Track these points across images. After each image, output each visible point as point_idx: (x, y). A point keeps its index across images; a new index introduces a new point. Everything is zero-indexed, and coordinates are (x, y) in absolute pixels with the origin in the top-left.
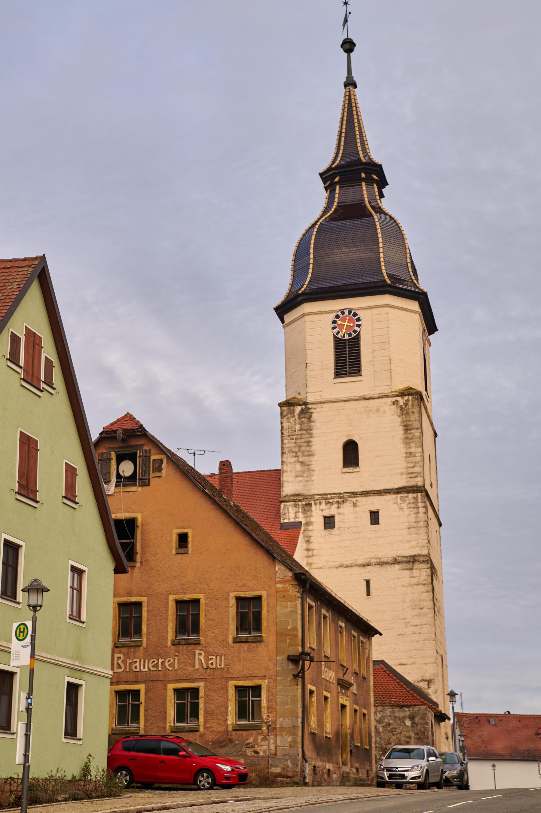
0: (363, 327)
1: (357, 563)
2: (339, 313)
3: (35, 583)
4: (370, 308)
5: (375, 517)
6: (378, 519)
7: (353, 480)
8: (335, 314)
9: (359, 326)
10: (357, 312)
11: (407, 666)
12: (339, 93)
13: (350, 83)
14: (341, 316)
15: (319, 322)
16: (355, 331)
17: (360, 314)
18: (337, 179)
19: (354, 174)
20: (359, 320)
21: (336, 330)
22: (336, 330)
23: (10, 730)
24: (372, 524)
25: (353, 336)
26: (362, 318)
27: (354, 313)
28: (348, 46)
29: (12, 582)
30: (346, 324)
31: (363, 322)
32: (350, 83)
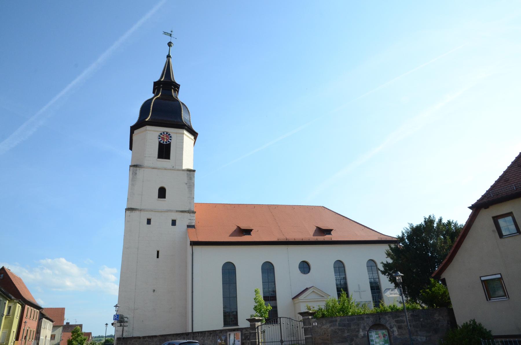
1: (139, 212)
3: (78, 327)
4: (176, 133)
5: (149, 222)
7: (162, 204)
9: (171, 139)
11: (142, 213)
13: (169, 56)
15: (152, 135)
17: (172, 135)
19: (166, 86)
20: (171, 137)
21: (160, 139)
22: (160, 139)
23: (237, 324)
24: (172, 225)
28: (170, 44)
29: (19, 315)
31: (173, 138)
32: (169, 56)
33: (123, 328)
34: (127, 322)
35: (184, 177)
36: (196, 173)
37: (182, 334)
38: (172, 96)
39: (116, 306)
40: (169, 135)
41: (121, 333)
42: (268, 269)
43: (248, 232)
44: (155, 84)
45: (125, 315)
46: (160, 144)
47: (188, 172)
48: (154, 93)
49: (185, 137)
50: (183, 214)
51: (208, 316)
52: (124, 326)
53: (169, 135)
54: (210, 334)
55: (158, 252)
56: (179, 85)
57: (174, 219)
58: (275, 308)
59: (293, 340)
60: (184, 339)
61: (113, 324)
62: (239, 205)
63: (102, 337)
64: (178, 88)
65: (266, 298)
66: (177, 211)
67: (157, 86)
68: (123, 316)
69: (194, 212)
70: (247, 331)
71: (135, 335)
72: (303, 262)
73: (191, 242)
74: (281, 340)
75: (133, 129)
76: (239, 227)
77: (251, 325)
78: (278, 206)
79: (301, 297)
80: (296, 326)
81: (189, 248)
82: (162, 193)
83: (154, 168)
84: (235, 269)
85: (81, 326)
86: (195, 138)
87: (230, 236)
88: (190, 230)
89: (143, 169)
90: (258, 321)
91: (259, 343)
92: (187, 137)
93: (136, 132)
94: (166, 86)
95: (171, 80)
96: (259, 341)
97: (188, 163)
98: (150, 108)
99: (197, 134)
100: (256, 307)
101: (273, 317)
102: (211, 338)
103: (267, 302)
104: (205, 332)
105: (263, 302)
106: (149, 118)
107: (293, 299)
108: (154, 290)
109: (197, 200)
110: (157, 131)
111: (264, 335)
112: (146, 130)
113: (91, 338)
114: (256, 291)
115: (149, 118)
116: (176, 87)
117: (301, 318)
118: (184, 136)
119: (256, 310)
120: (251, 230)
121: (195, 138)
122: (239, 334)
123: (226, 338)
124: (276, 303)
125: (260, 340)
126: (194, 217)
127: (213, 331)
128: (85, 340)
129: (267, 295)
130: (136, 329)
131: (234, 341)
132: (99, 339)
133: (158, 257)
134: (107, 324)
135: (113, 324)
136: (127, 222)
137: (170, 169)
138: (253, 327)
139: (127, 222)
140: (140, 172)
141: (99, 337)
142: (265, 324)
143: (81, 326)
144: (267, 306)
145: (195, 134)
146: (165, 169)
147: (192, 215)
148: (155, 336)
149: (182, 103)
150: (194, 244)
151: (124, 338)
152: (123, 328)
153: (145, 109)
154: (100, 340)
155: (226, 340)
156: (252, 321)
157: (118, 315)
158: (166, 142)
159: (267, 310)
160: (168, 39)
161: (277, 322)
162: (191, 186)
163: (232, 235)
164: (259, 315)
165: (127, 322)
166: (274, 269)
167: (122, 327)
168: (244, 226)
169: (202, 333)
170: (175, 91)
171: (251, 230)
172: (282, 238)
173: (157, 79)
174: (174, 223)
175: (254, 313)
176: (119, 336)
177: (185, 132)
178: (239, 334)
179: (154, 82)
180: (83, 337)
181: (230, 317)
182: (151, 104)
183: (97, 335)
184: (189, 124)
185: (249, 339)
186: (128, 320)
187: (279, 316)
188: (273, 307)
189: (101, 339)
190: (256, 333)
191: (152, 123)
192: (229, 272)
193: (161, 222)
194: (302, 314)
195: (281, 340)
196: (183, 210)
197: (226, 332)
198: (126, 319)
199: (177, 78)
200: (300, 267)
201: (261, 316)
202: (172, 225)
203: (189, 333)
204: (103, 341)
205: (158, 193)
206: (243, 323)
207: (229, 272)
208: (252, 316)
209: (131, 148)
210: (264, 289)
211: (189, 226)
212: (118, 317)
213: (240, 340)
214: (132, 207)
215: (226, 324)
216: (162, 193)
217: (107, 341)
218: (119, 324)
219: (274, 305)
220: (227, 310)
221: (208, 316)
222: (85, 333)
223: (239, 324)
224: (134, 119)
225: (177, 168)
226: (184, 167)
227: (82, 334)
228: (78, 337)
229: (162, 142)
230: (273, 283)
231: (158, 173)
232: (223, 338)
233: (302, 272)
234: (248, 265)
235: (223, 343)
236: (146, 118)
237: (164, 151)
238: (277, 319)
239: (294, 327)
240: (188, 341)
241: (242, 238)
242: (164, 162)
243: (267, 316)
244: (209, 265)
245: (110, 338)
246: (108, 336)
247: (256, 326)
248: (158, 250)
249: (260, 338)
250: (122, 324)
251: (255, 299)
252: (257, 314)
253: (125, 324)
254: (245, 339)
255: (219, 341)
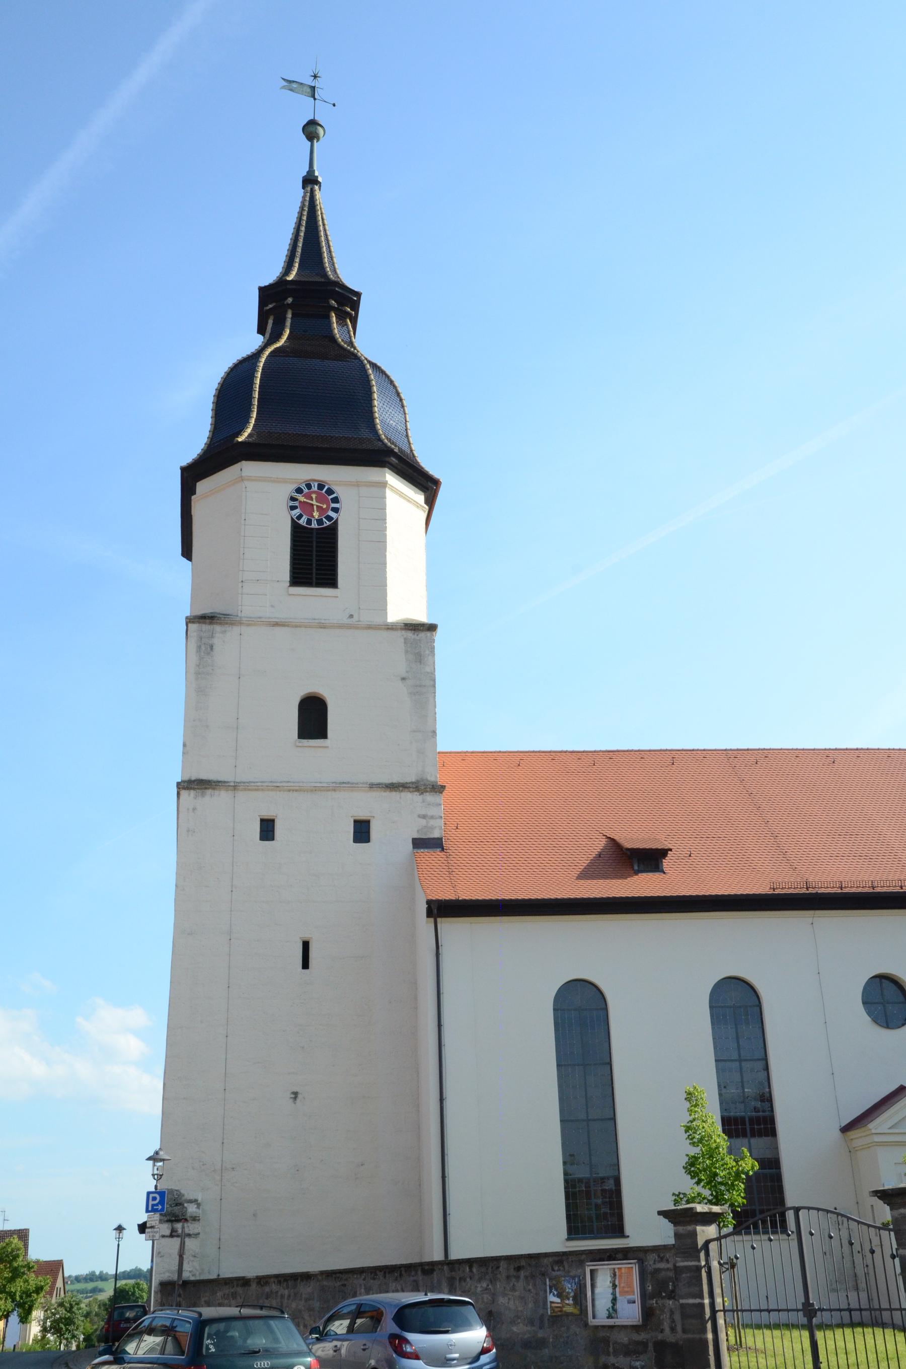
0: (342, 512)
1: (230, 793)
2: (303, 486)
3: (15, 1240)
4: (357, 484)
5: (267, 829)
6: (368, 832)
8: (295, 486)
9: (336, 510)
10: (334, 488)
11: (241, 795)
12: (298, 194)
13: (310, 181)
14: (306, 490)
15: (264, 496)
16: (329, 518)
17: (339, 491)
18: (290, 300)
19: (308, 301)
20: (336, 500)
21: (297, 512)
22: (297, 512)
23: (618, 1230)
24: (356, 840)
25: (325, 525)
26: (342, 498)
27: (329, 489)
28: (311, 130)
30: (314, 502)
31: (344, 505)
32: (310, 181)
33: (182, 1245)
34: (195, 1219)
35: (395, 651)
36: (439, 637)
37: (409, 1268)
38: (333, 339)
39: (154, 1158)
40: (330, 492)
41: (175, 1267)
42: (737, 1008)
43: (650, 859)
44: (267, 294)
45: (188, 1194)
46: (296, 529)
47: (409, 634)
48: (261, 330)
49: (391, 498)
50: (395, 795)
51: (510, 1203)
52: (184, 1236)
53: (327, 493)
54: (518, 1269)
55: (306, 945)
56: (358, 295)
57: (362, 815)
58: (771, 1166)
59: (854, 1305)
60: (416, 1289)
61: (142, 1228)
62: (611, 754)
63: (103, 1277)
64: (355, 306)
65: (733, 1126)
66: (372, 786)
67: (273, 300)
68: (180, 1195)
69: (438, 789)
70: (661, 1259)
71: (226, 1273)
72: (882, 978)
73: (429, 902)
74: (807, 1304)
75: (192, 475)
76: (613, 843)
77: (677, 1235)
78: (766, 754)
79: (881, 1124)
80: (867, 1248)
81: (425, 926)
82: (313, 718)
83: (276, 624)
84: (605, 1009)
85: (23, 1235)
86: (430, 501)
87: (579, 877)
88: (426, 855)
89: (236, 629)
90: (708, 1219)
91: (714, 1312)
92: (400, 499)
93: (202, 486)
94: (308, 301)
95: (325, 275)
96: (712, 1304)
97: (405, 602)
98: (251, 390)
99: (436, 483)
100: (692, 1162)
101: (763, 1206)
102: (520, 1285)
103: (738, 1141)
104: (497, 1259)
105: (721, 1140)
106: (249, 430)
107: (845, 1129)
108: (295, 1095)
109: (448, 740)
110: (285, 481)
111: (732, 1278)
112: (242, 479)
113: (59, 1283)
114: (689, 1096)
115: (249, 430)
116: (347, 302)
117: (885, 1213)
118: (388, 492)
119: (693, 1175)
120: (664, 853)
121: (430, 501)
122: (631, 1270)
123: (581, 1288)
124: (776, 1148)
125: (719, 1300)
126: (436, 806)
127: (530, 1257)
128: (39, 1290)
129: (738, 1111)
130: (227, 1251)
131: (614, 1300)
132: (90, 1286)
133: (306, 965)
134: (120, 1229)
135: (142, 1228)
136: (186, 833)
137: (341, 626)
138: (687, 1246)
139: (185, 833)
140: (226, 641)
141: (91, 1277)
142: (737, 1231)
143: (23, 1235)
144: (739, 1158)
145: (426, 484)
146: (323, 626)
147: (430, 797)
148: (306, 1277)
149: (374, 366)
150: (441, 910)
151: (186, 1283)
152: (182, 1245)
153: (231, 395)
154: (95, 1290)
155: (579, 1297)
156: (682, 1217)
157: (162, 1194)
158: (320, 522)
159: (738, 1174)
160: (303, 109)
161: (784, 1229)
162: (421, 686)
163: (587, 874)
164: (706, 1193)
165: (195, 1219)
166: (759, 1005)
167: (176, 1242)
168: (634, 837)
169: (487, 1266)
170: (342, 317)
171: (664, 853)
172: (788, 881)
173: (270, 276)
174: (362, 831)
175: (687, 1185)
176: (166, 1277)
177: (391, 479)
178: (631, 1270)
179: (261, 289)
180: (33, 1280)
181: (593, 1201)
182: (252, 377)
183: (83, 1271)
184: (405, 448)
185: (672, 1295)
186: (199, 1212)
187: (792, 1198)
188: (763, 1163)
189: (100, 1284)
190: (699, 1269)
191: (260, 451)
192: (582, 1016)
193: (315, 830)
194: (885, 1196)
195: (807, 1304)
196: (396, 779)
197: (582, 1264)
198: (191, 1209)
199: (347, 266)
200: (868, 1001)
201: (717, 1201)
202: (356, 840)
203: (433, 1264)
204: (108, 1292)
205: (298, 720)
206: (645, 1227)
207: (582, 1016)
208: (678, 1197)
209: (187, 552)
210: (722, 1086)
211: (419, 843)
212: (162, 1202)
213: (636, 1296)
214: (204, 776)
215: (575, 1229)
216: (313, 718)
217: (120, 1294)
218: (165, 1229)
219: (768, 1155)
220: (582, 1172)
221: (510, 1203)
222: (37, 1262)
223: (628, 1229)
224: (194, 441)
225: (366, 618)
226: (396, 613)
227: (29, 1267)
228: (12, 1280)
229: (303, 522)
230: (760, 1065)
231: (294, 642)
232: (569, 1287)
233: (875, 1021)
234: (656, 987)
235: (570, 1307)
236: (239, 433)
237: (315, 557)
238: (783, 1215)
239: (856, 1247)
240: (431, 1296)
241: (629, 879)
242: (314, 598)
243: (739, 1197)
244: (506, 987)
245: (131, 1282)
246: (127, 1275)
247: (700, 1242)
248: (306, 936)
249: (717, 1291)
250: (179, 1226)
251: (688, 1129)
252: (698, 1189)
253: (191, 1228)
254: (656, 1294)
255: (552, 1298)
